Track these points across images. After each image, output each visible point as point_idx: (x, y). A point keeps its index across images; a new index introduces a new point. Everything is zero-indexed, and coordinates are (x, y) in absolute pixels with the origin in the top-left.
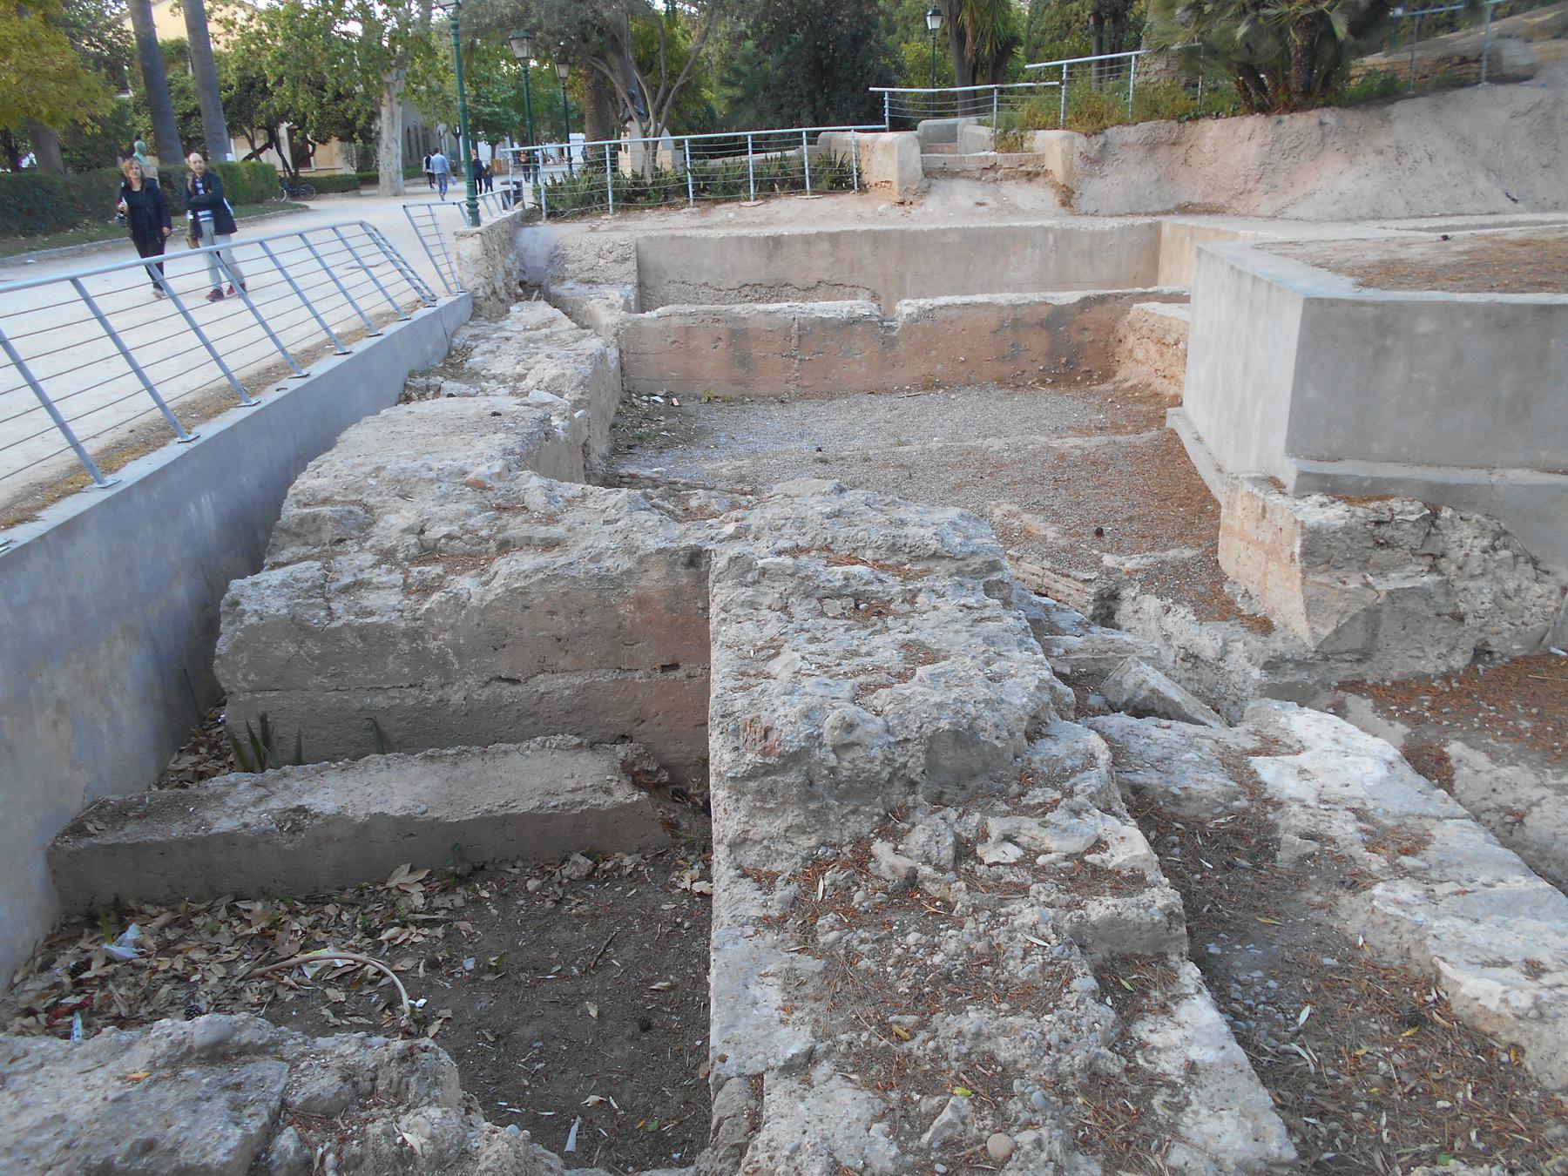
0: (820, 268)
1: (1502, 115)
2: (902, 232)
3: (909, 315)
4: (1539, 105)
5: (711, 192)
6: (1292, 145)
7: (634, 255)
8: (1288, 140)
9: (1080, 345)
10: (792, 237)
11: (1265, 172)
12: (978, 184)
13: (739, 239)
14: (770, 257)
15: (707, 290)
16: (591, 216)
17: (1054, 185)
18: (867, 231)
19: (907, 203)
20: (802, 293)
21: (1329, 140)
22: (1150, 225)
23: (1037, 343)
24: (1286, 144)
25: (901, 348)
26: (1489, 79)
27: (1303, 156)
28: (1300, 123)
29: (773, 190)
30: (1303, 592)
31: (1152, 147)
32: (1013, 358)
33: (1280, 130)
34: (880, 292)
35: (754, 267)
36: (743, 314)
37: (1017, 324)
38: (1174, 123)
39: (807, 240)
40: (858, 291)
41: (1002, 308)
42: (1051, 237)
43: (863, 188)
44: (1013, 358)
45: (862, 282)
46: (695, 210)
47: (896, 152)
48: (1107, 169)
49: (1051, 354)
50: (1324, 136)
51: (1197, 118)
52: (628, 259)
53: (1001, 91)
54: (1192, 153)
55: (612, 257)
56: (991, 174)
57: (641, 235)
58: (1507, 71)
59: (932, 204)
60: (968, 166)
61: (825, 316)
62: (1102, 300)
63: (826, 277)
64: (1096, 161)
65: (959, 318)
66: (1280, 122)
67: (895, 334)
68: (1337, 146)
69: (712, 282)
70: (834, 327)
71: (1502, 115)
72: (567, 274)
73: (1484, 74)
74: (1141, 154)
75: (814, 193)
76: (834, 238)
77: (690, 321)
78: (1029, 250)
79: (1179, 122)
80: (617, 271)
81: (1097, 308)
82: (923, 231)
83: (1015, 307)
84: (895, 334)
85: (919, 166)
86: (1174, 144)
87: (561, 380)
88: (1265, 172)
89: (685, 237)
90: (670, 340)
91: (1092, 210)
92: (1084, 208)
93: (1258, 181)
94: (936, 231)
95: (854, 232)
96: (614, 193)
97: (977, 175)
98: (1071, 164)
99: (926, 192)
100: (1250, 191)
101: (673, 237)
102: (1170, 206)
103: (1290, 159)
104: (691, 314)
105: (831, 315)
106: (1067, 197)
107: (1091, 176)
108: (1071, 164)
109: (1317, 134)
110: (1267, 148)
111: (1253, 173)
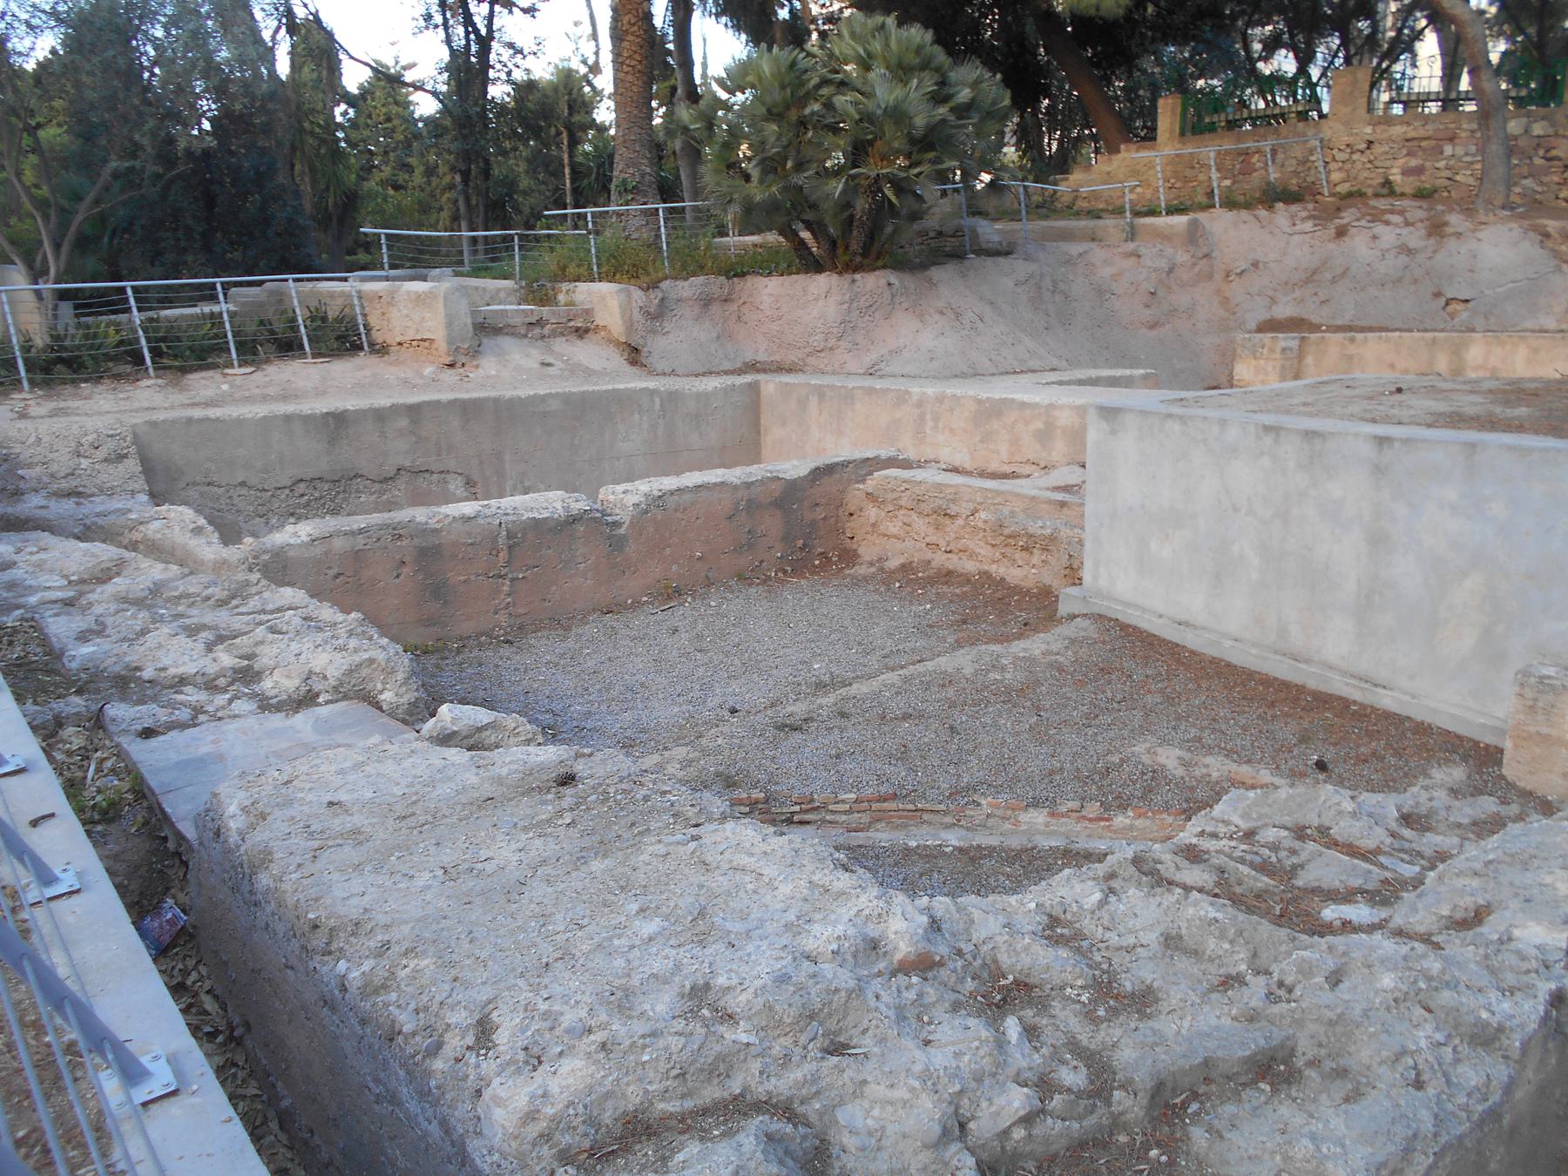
0: (399, 451)
1: (1009, 283)
2: (496, 401)
3: (636, 505)
4: (1032, 276)
5: (175, 357)
7: (133, 450)
8: (864, 298)
9: (813, 523)
10: (361, 414)
11: (846, 328)
12: (526, 341)
13: (288, 418)
14: (332, 442)
15: (244, 491)
17: (611, 341)
18: (455, 401)
20: (377, 486)
21: (897, 300)
22: (750, 385)
23: (772, 525)
24: (862, 302)
25: (631, 549)
26: (974, 252)
27: (877, 314)
28: (872, 282)
29: (255, 353)
31: (706, 302)
32: (751, 546)
33: (856, 289)
34: (476, 477)
35: (312, 456)
36: (433, 524)
37: (753, 506)
38: (723, 279)
39: (380, 416)
40: (449, 477)
41: (735, 488)
42: (657, 401)
43: (380, 350)
44: (751, 546)
45: (451, 464)
46: (160, 381)
47: (441, 306)
48: (668, 326)
49: (787, 538)
50: (893, 296)
51: (743, 275)
52: (125, 456)
53: (521, 237)
54: (745, 309)
55: (101, 454)
56: (537, 331)
57: (139, 419)
58: (985, 246)
59: (488, 366)
60: (512, 322)
61: (537, 515)
62: (830, 469)
63: (407, 463)
64: (657, 315)
65: (692, 504)
66: (853, 281)
67: (622, 531)
68: (905, 305)
69: (253, 481)
70: (551, 530)
71: (1009, 283)
72: (22, 485)
73: (968, 248)
74: (696, 310)
75: (371, 353)
76: (414, 411)
77: (360, 541)
78: (637, 416)
79: (728, 278)
80: (113, 475)
81: (826, 480)
82: (519, 398)
83: (748, 485)
84: (622, 531)
85: (469, 321)
86: (726, 301)
87: (365, 672)
88: (846, 328)
89: (208, 419)
90: (332, 572)
91: (668, 370)
92: (659, 368)
93: (839, 338)
94: (536, 397)
95: (438, 402)
96: (26, 360)
97: (523, 332)
98: (631, 318)
99: (475, 352)
100: (831, 349)
101: (190, 421)
103: (867, 318)
104: (361, 531)
105: (546, 515)
106: (634, 354)
107: (653, 332)
108: (631, 318)
109: (887, 294)
110: (846, 306)
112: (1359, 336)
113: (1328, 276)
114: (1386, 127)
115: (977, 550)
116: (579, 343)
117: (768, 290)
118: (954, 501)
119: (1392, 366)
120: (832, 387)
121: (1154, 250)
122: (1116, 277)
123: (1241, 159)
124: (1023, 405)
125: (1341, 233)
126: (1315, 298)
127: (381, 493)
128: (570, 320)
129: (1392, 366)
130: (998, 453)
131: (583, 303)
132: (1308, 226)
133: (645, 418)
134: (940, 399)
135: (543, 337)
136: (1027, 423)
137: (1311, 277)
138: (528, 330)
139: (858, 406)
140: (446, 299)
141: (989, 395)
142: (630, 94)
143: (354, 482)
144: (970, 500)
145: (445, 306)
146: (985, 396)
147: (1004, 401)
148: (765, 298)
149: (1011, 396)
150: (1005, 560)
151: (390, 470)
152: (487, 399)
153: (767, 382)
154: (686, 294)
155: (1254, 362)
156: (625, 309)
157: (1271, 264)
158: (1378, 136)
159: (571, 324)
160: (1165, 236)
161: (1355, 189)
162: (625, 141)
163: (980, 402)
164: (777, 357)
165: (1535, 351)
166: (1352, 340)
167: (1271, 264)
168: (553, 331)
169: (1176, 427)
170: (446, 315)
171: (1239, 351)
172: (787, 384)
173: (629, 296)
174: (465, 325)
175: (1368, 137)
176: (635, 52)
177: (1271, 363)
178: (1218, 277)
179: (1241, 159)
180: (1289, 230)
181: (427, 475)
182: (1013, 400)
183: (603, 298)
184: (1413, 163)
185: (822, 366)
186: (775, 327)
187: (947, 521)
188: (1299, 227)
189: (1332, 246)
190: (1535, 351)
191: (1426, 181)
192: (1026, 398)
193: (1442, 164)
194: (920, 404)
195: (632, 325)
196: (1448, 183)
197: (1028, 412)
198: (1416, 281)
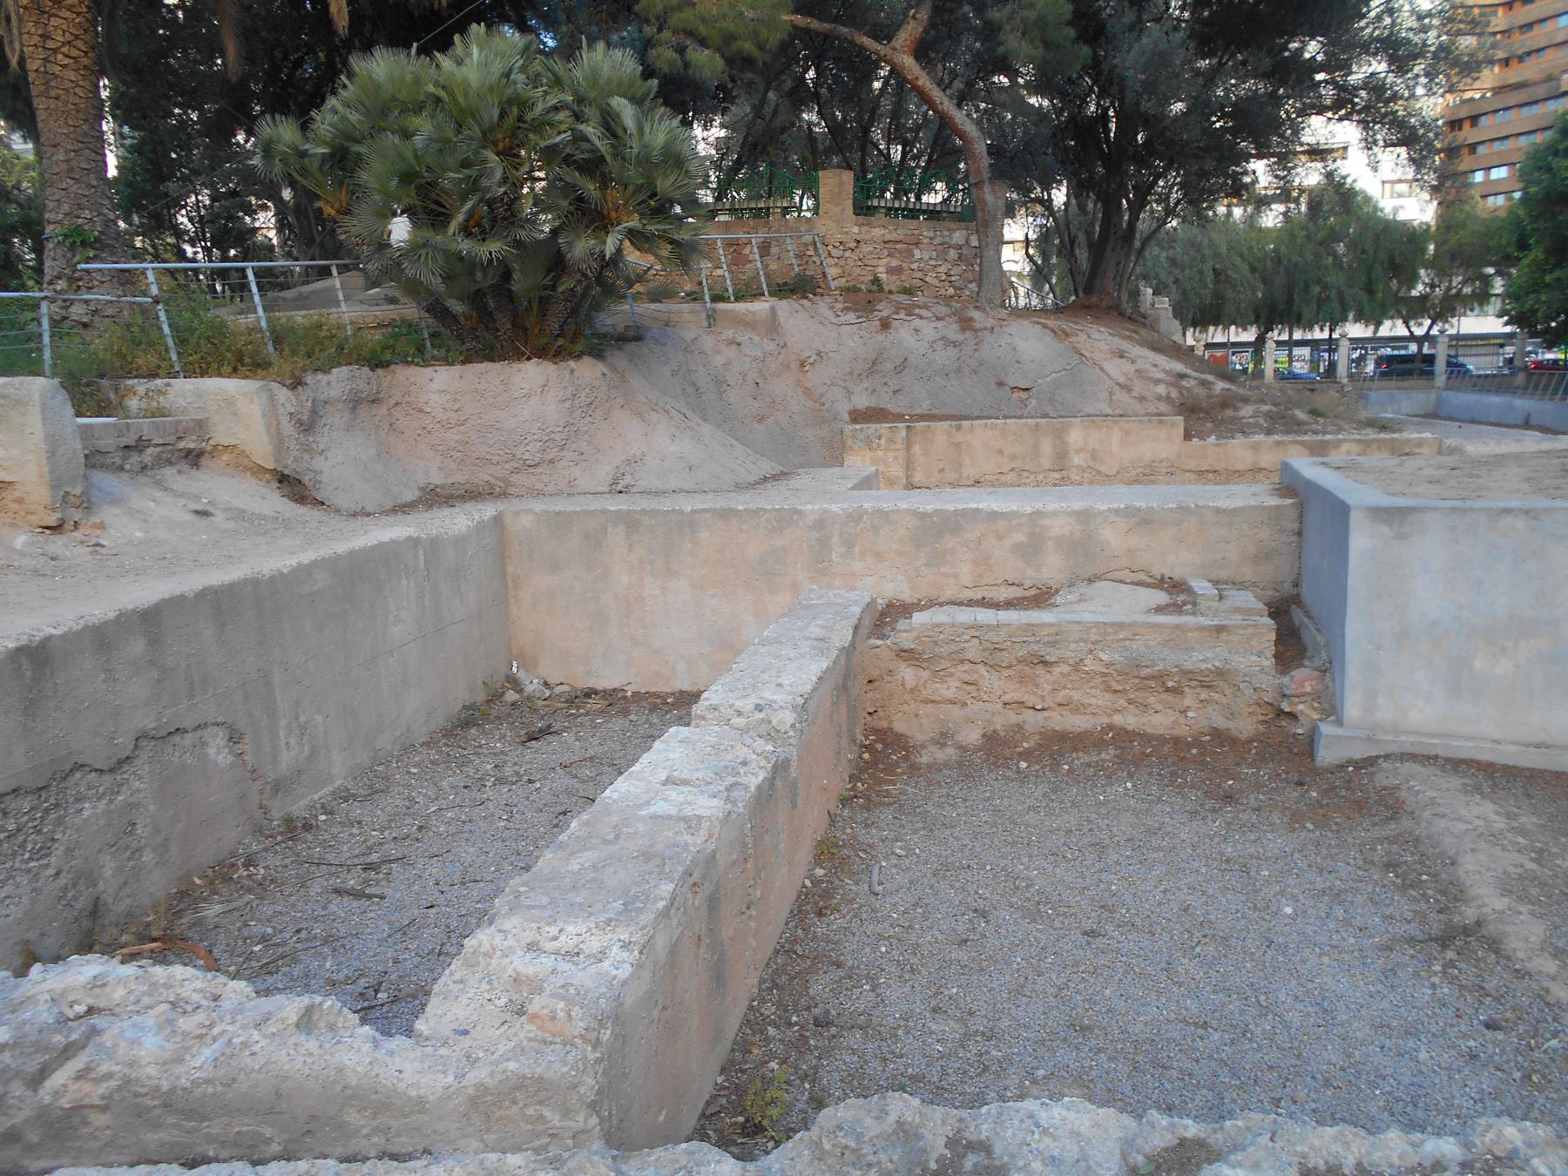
6: (589, 401)
16: (1333, 695)
19: (69, 525)
30: (57, 959)
38: (366, 369)
56: (135, 458)
63: (150, 724)
66: (572, 371)
74: (347, 417)
76: (150, 620)
86: (373, 401)
93: (563, 448)
100: (551, 461)
102: (409, 495)
106: (292, 485)
110: (568, 403)
111: (557, 437)
112: (965, 423)
113: (889, 366)
114: (867, 228)
115: (1086, 701)
116: (194, 472)
117: (435, 386)
118: (1053, 644)
119: (1000, 452)
120: (653, 513)
121: (708, 342)
122: (727, 365)
123: (732, 250)
124: (993, 516)
125: (885, 325)
126: (886, 388)
127: (114, 791)
128: (179, 438)
129: (1000, 452)
130: (956, 577)
131: (184, 411)
132: (851, 317)
133: (412, 583)
134: (856, 517)
135: (144, 468)
136: (1000, 537)
137: (873, 367)
138: (124, 459)
139: (704, 535)
140: (43, 405)
141: (938, 507)
142: (72, 99)
143: (72, 780)
144: (1081, 640)
145: (44, 419)
146: (929, 508)
147: (964, 513)
148: (434, 397)
149: (973, 506)
150: (1132, 707)
151: (125, 742)
152: (244, 582)
153: (517, 513)
154: (334, 393)
155: (869, 454)
156: (271, 413)
157: (830, 355)
158: (864, 237)
159: (182, 445)
160: (747, 323)
161: (851, 284)
162: (71, 170)
163: (924, 516)
164: (459, 478)
165: (1127, 433)
166: (959, 428)
167: (830, 355)
168: (158, 457)
169: (1520, 523)
170: (47, 436)
171: (849, 442)
172: (558, 514)
173: (272, 398)
174: (74, 452)
175: (855, 237)
176: (77, 37)
177: (891, 454)
178: (794, 366)
179: (732, 250)
180: (835, 321)
181: (176, 738)
182: (978, 511)
183: (229, 402)
184: (894, 263)
185: (540, 486)
186: (452, 436)
187: (1040, 670)
188: (842, 318)
189: (880, 337)
190: (1127, 433)
191: (907, 280)
192: (995, 506)
193: (915, 266)
194: (820, 524)
195: (281, 442)
196: (921, 283)
197: (1002, 523)
198: (975, 371)
